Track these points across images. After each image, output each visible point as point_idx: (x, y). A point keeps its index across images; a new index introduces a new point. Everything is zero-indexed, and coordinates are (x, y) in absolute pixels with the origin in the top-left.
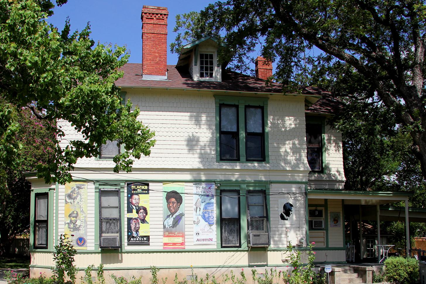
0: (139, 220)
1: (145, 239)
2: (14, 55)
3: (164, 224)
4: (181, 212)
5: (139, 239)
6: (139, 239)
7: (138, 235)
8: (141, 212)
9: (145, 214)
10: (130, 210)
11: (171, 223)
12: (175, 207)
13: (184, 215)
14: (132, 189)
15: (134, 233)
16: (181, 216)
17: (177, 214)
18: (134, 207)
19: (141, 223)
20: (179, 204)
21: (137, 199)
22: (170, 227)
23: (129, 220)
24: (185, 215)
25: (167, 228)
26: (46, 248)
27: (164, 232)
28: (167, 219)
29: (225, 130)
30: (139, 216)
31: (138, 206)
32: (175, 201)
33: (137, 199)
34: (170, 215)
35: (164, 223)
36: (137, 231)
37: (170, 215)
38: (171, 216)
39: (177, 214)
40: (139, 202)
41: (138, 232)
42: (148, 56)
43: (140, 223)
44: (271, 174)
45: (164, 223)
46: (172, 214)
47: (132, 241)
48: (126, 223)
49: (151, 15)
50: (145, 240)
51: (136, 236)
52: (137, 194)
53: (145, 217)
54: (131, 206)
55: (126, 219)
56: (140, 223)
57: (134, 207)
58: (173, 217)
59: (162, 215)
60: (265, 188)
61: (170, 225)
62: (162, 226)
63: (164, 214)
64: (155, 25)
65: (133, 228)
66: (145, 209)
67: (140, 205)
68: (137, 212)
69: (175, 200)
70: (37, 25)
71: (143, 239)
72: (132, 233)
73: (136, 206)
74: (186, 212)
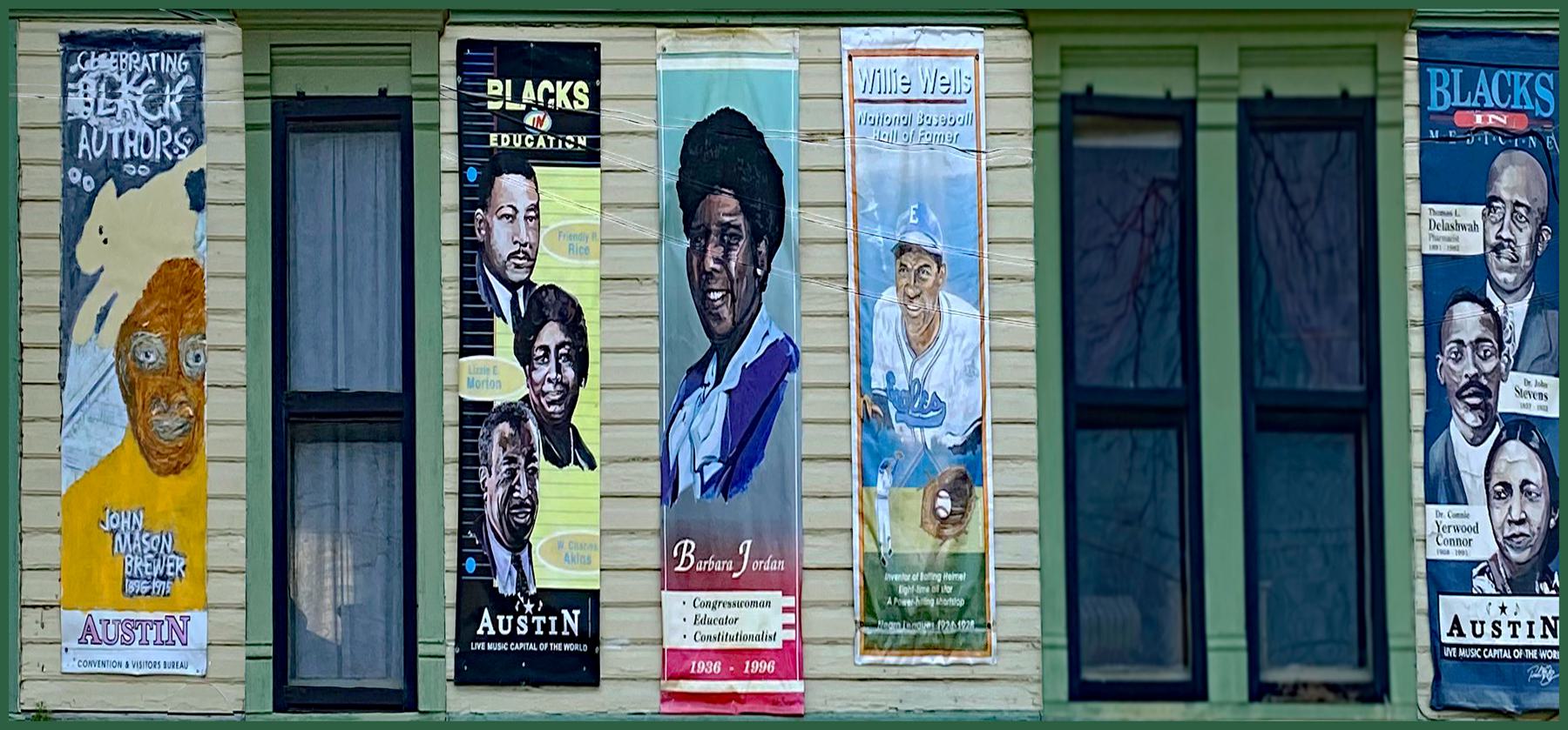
0: (532, 425)
1: (571, 619)
2: (737, 244)
3: (664, 458)
5: (532, 627)
6: (532, 627)
7: (522, 584)
8: (546, 348)
10: (476, 340)
11: (711, 445)
12: (741, 273)
13: (792, 364)
16: (782, 358)
17: (749, 351)
18: (503, 295)
19: (550, 457)
22: (704, 488)
23: (475, 416)
24: (805, 358)
27: (672, 535)
29: (1147, 438)
30: (532, 383)
31: (528, 284)
32: (740, 220)
37: (701, 367)
38: (712, 368)
39: (749, 351)
40: (535, 247)
41: (524, 554)
43: (543, 464)
46: (723, 347)
47: (487, 638)
48: (451, 438)
51: (510, 591)
54: (480, 281)
55: (451, 413)
56: (543, 464)
57: (503, 295)
59: (653, 360)
60: (1366, 72)
62: (650, 477)
63: (669, 347)
65: (492, 510)
67: (539, 278)
69: (733, 204)
73: (512, 286)
74: (803, 341)
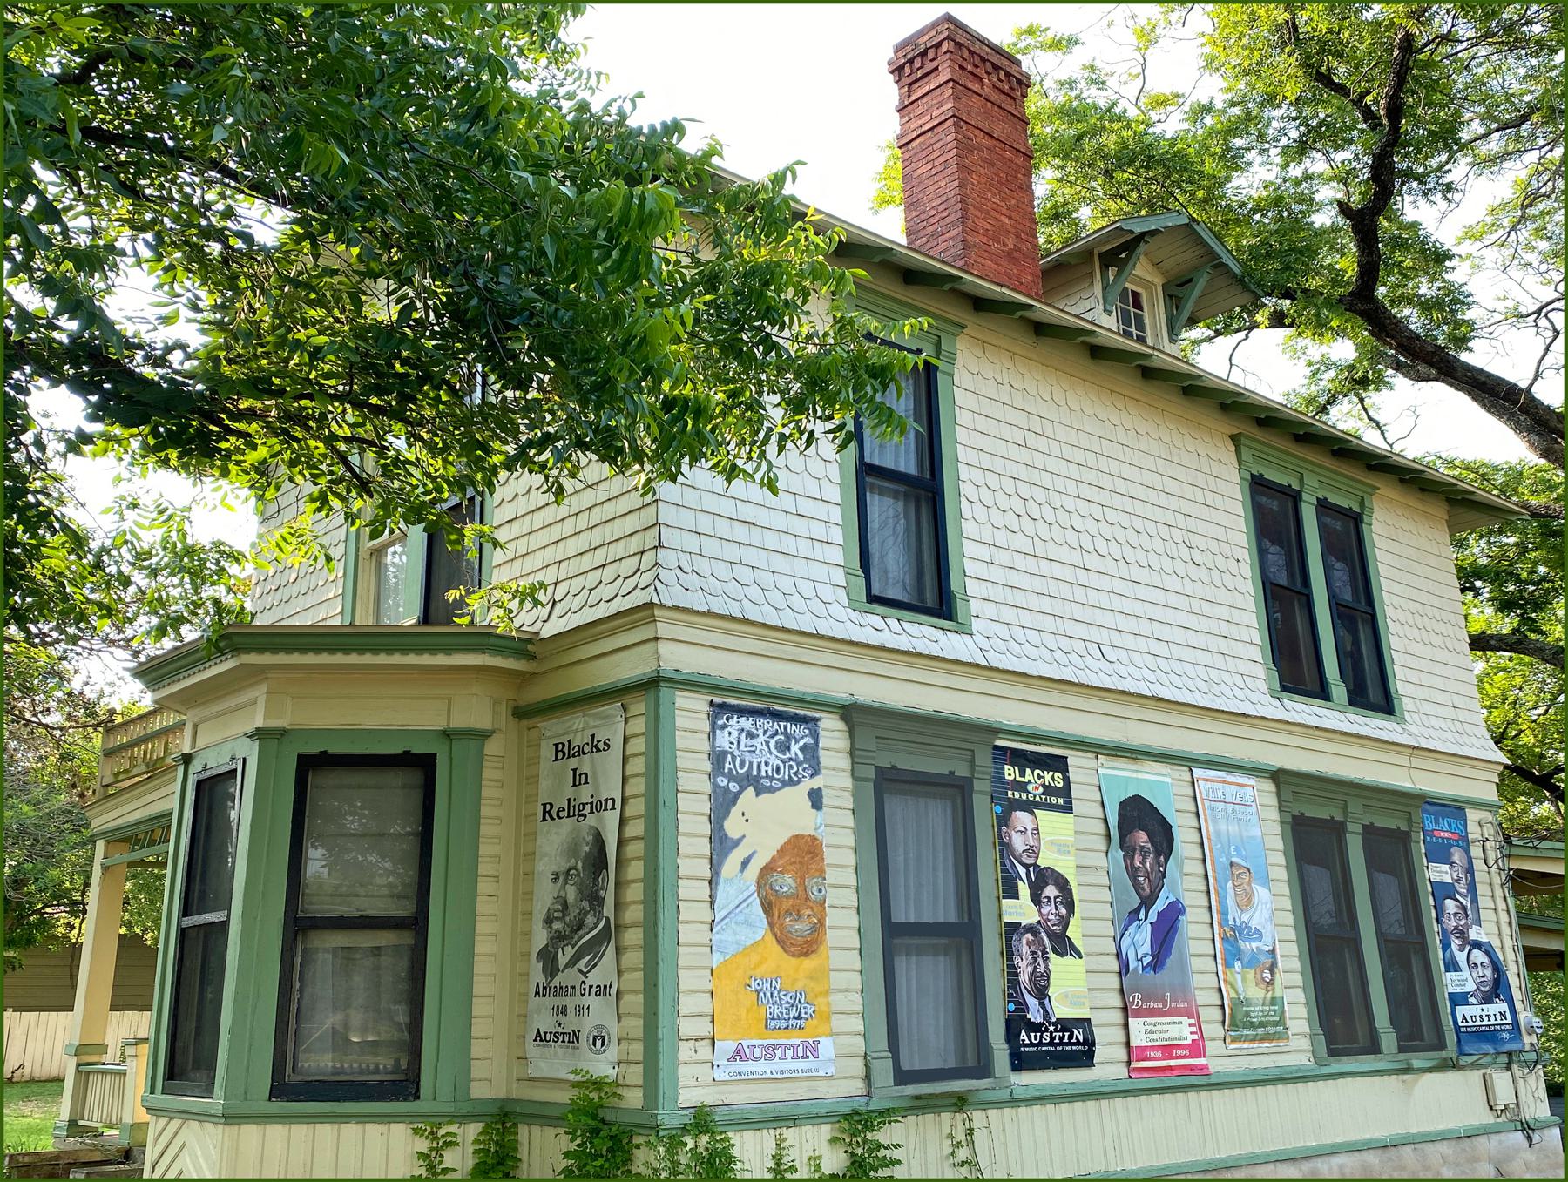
3: (1118, 955)
4: (1172, 898)
5: (1052, 1038)
6: (1052, 1038)
7: (1046, 1015)
9: (1063, 911)
11: (1147, 948)
13: (1182, 912)
14: (11, 602)
15: (1032, 1002)
17: (1160, 904)
18: (1022, 871)
19: (1055, 951)
20: (1162, 858)
21: (1029, 832)
22: (1144, 968)
25: (1136, 969)
26: (309, 765)
28: (1132, 929)
31: (1035, 866)
33: (1029, 832)
34: (1137, 911)
35: (1119, 948)
36: (1042, 994)
37: (1137, 911)
39: (1160, 904)
42: (978, 214)
43: (1052, 955)
44: (1416, 762)
45: (1119, 948)
49: (977, 61)
50: (1078, 1043)
51: (1040, 1020)
52: (1028, 807)
53: (1064, 921)
56: (1052, 955)
57: (1022, 871)
58: (1148, 921)
61: (1145, 955)
64: (989, 105)
65: (1024, 978)
66: (1063, 884)
67: (1042, 863)
68: (1036, 899)
70: (176, 612)
71: (1071, 1037)
72: (1022, 1007)
73: (1026, 866)
